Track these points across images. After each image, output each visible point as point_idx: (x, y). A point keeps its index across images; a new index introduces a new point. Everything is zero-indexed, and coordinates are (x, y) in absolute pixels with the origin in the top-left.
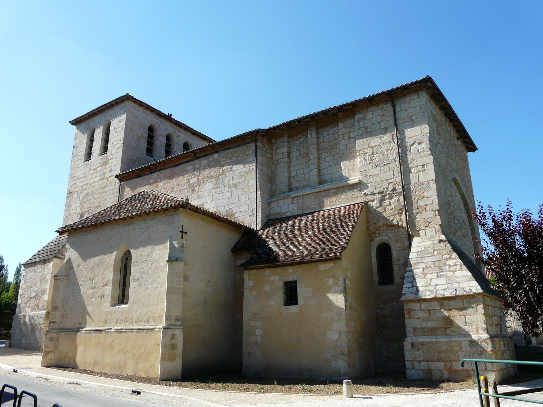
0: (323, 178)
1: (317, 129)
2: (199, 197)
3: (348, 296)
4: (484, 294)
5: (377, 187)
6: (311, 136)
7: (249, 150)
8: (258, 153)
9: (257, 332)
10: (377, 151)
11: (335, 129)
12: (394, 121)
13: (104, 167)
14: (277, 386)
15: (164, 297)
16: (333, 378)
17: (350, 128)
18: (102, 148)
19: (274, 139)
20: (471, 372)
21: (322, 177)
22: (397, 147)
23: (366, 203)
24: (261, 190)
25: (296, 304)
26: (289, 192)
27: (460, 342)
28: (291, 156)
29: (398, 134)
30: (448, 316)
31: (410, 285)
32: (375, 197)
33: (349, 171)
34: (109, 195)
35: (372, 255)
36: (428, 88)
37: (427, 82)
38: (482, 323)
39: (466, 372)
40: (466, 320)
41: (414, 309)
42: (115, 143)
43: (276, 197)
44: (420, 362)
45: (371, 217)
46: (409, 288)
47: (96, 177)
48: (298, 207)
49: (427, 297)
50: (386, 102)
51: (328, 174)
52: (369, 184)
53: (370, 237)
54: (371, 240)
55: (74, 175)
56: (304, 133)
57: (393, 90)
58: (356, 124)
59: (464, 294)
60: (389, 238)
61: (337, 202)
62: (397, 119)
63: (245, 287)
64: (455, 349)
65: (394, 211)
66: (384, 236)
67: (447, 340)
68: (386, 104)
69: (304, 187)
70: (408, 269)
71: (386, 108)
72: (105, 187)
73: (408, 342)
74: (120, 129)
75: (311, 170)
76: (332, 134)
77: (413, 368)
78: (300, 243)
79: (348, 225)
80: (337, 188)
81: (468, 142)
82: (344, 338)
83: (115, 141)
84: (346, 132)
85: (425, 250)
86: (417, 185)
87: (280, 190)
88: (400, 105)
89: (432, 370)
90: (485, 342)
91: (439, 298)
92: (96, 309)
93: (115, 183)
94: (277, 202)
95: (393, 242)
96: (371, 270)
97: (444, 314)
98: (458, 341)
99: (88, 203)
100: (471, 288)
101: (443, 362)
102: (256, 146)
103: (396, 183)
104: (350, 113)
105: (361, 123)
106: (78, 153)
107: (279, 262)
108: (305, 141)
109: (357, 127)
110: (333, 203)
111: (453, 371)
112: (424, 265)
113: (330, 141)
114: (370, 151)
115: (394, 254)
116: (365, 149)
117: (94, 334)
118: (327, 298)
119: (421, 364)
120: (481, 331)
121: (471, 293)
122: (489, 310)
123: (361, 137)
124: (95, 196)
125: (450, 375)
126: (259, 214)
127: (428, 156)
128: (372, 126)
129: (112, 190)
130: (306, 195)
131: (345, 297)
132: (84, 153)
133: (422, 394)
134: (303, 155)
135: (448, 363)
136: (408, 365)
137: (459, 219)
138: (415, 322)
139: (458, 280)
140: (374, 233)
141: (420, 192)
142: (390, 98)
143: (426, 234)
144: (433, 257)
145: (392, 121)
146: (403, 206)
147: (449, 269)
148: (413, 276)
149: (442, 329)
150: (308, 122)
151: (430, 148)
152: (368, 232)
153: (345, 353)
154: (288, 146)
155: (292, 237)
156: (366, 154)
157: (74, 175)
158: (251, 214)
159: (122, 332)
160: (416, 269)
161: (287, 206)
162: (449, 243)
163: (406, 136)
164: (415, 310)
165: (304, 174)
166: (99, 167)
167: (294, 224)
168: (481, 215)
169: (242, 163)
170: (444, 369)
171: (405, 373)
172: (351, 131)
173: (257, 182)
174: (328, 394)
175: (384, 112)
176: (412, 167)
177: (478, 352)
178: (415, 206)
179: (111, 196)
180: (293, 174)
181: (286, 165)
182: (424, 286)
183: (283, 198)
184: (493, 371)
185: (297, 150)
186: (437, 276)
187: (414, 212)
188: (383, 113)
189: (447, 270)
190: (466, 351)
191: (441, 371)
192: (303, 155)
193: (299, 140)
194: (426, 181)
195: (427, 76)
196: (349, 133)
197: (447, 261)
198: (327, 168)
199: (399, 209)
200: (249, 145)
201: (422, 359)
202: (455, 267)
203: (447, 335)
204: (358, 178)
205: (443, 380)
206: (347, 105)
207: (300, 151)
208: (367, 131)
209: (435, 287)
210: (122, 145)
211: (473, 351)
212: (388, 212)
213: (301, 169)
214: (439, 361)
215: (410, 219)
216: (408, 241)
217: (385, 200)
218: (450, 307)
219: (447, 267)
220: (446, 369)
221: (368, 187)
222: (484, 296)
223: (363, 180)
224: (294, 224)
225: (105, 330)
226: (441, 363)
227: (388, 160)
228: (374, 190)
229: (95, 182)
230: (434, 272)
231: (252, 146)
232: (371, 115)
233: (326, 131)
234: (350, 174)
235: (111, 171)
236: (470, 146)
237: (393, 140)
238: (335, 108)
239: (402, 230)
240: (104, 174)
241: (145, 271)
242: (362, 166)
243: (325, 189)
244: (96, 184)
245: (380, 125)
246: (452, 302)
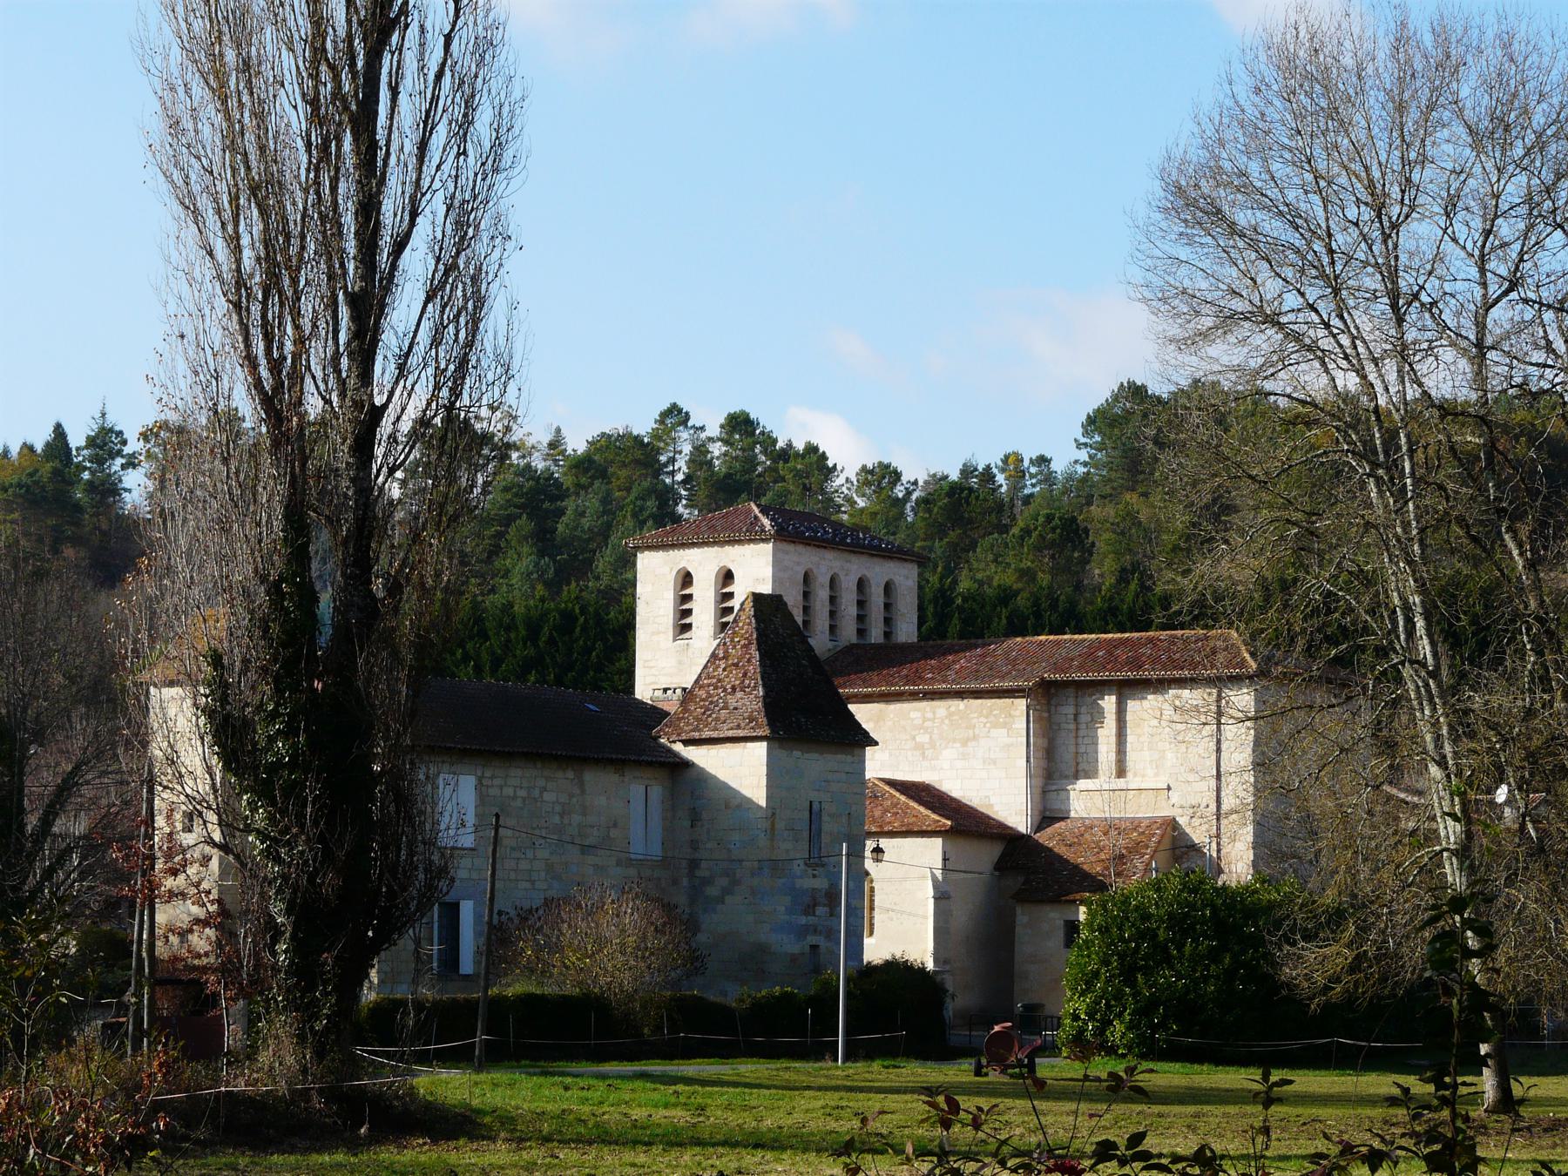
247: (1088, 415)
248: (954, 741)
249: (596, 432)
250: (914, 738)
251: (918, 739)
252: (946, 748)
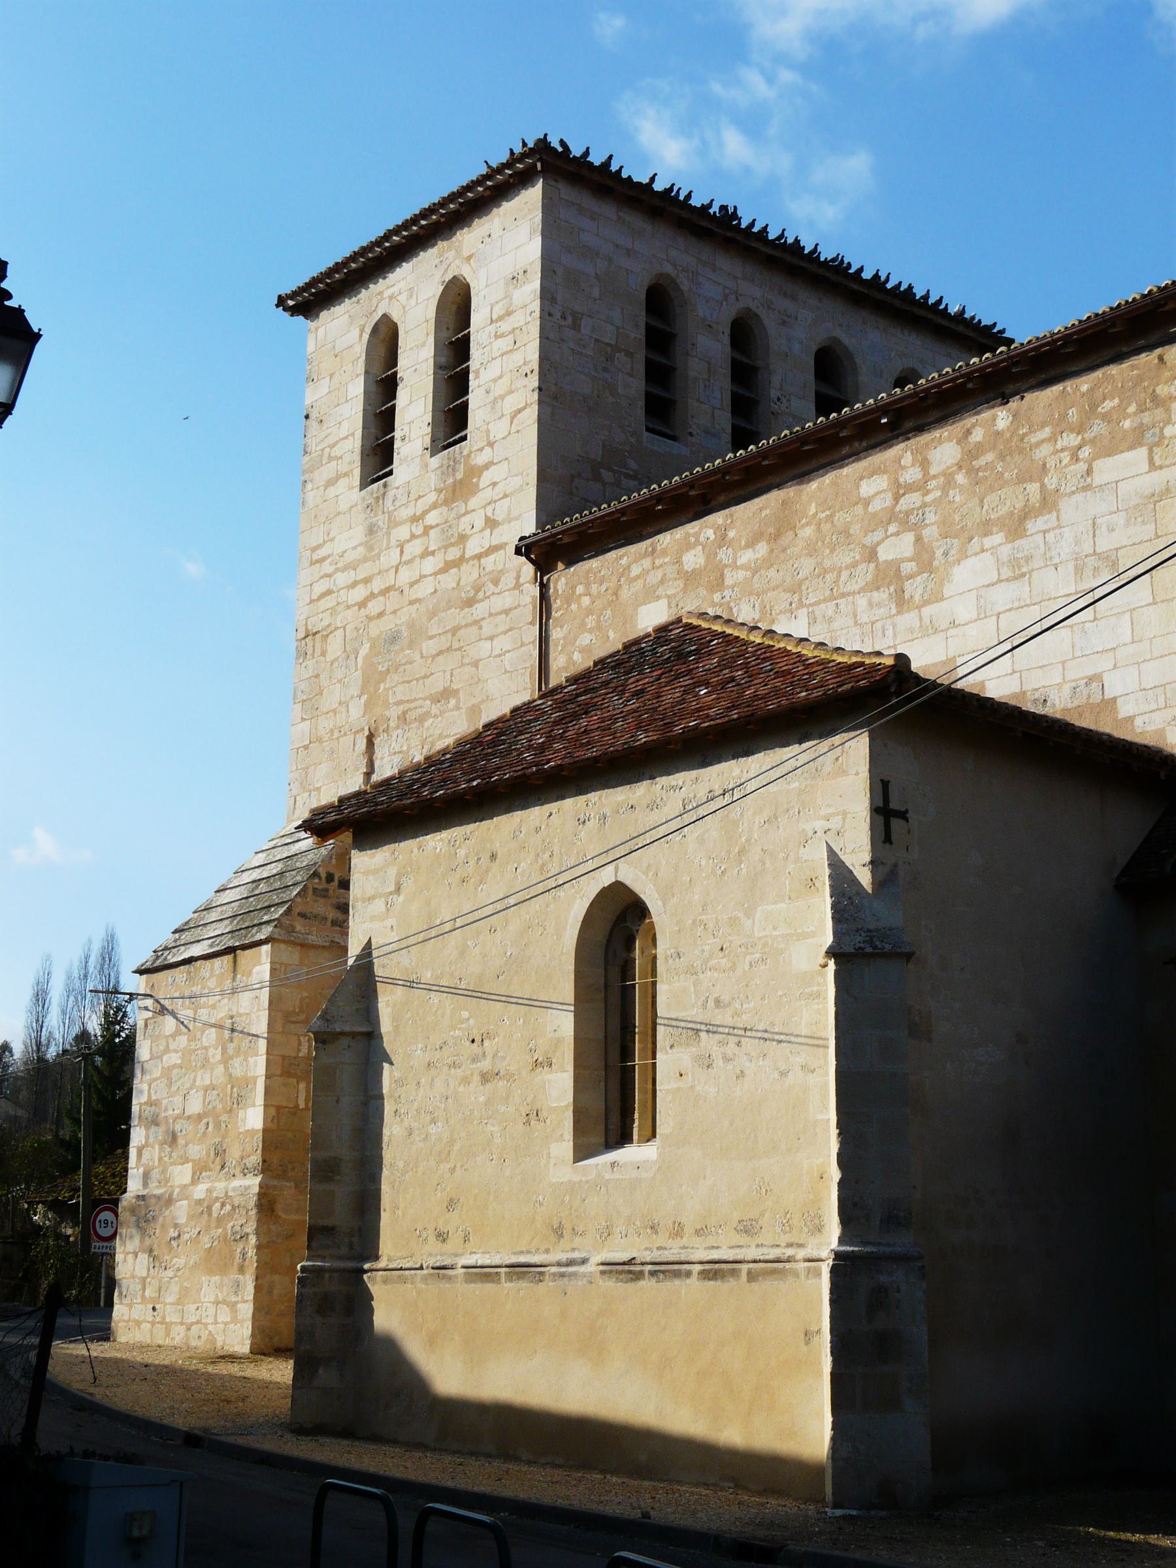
2: (930, 629)
13: (460, 506)
15: (819, 1117)
18: (442, 417)
34: (491, 638)
42: (499, 389)
47: (426, 553)
55: (321, 553)
72: (470, 602)
74: (518, 319)
83: (501, 377)
92: (508, 1173)
93: (518, 577)
99: (395, 677)
106: (332, 446)
117: (509, 1285)
124: (429, 647)
129: (506, 612)
132: (358, 443)
157: (321, 553)
159: (638, 1276)
166: (434, 506)
179: (503, 643)
210: (536, 396)
225: (559, 1264)
229: (422, 577)
235: (491, 523)
240: (463, 538)
241: (725, 998)
244: (425, 589)
247: (292, 315)
248: (986, 528)
249: (451, 191)
250: (871, 554)
251: (884, 554)
252: (964, 555)
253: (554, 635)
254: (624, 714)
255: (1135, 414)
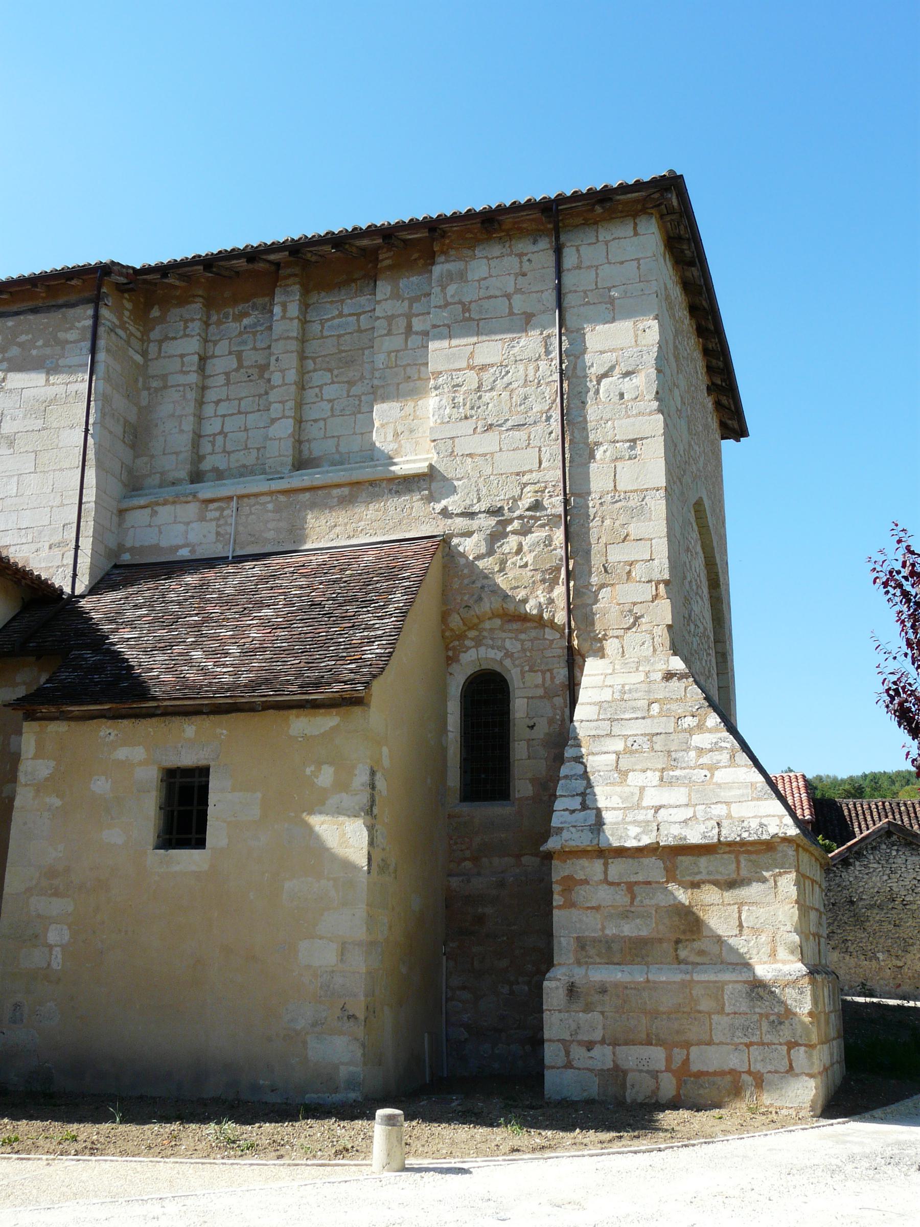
0: (311, 453)
1: (306, 291)
3: (377, 827)
4: (805, 842)
5: (484, 491)
6: (285, 310)
7: (71, 329)
8: (101, 343)
9: (53, 936)
10: (494, 381)
11: (362, 300)
12: (554, 294)
14: (122, 1128)
16: (311, 1097)
17: (413, 300)
19: (156, 307)
20: (745, 1077)
21: (307, 444)
22: (556, 376)
23: (445, 540)
24: (100, 466)
25: (200, 843)
26: (192, 482)
27: (720, 987)
28: (209, 370)
29: (564, 338)
30: (687, 903)
31: (576, 803)
32: (475, 524)
33: (396, 435)
35: (449, 703)
36: (665, 211)
37: (668, 190)
38: (789, 928)
39: (728, 1078)
40: (743, 918)
41: (584, 877)
43: (146, 495)
44: (590, 1046)
45: (456, 586)
46: (573, 811)
48: (218, 534)
49: (631, 843)
50: (535, 235)
51: (325, 437)
52: (460, 483)
53: (447, 648)
54: (448, 658)
56: (260, 301)
57: (561, 199)
58: (436, 290)
59: (742, 839)
60: (508, 655)
61: (350, 528)
62: (563, 292)
63: (22, 778)
64: (701, 1008)
65: (532, 573)
66: (493, 648)
67: (678, 977)
68: (535, 242)
69: (245, 471)
70: (569, 753)
71: (533, 253)
73: (558, 983)
75: (273, 421)
76: (350, 315)
77: (569, 1065)
78: (225, 644)
79: (388, 602)
80: (356, 484)
81: (729, 409)
82: (359, 964)
84: (399, 313)
85: (622, 700)
86: (608, 498)
87: (162, 474)
88: (578, 250)
89: (625, 1073)
90: (793, 988)
91: (664, 847)
94: (148, 510)
95: (519, 669)
96: (444, 750)
97: (675, 898)
98: (716, 982)
100: (764, 821)
101: (661, 1046)
102: (96, 317)
103: (546, 487)
104: (416, 255)
105: (451, 289)
107: (154, 699)
108: (261, 325)
109: (436, 299)
110: (337, 530)
111: (690, 1076)
112: (619, 745)
113: (343, 335)
114: (471, 379)
115: (519, 707)
116: (455, 370)
118: (309, 829)
119: (593, 1053)
120: (782, 953)
121: (765, 837)
122: (805, 890)
123: (448, 331)
125: (679, 1087)
126: (86, 544)
127: (650, 414)
128: (486, 304)
130: (248, 496)
131: (371, 829)
133: (622, 1153)
134: (250, 371)
135: (676, 1050)
136: (551, 1053)
137: (700, 625)
138: (584, 918)
139: (725, 795)
140: (461, 637)
141: (618, 523)
142: (550, 226)
143: (623, 652)
144: (648, 721)
145: (550, 297)
146: (561, 560)
147: (697, 761)
148: (585, 775)
149: (665, 945)
150: (277, 265)
151: (657, 393)
152: (443, 631)
153: (358, 1015)
154: (203, 335)
155: (197, 625)
156: (458, 385)
158: (56, 539)
160: (593, 754)
161: (181, 528)
162: (696, 682)
163: (587, 345)
164: (586, 882)
165: (246, 430)
167: (203, 586)
168: (905, 572)
169: (44, 368)
170: (663, 1068)
171: (540, 1078)
172: (414, 311)
173: (89, 437)
174: (314, 1156)
175: (526, 265)
176: (598, 444)
177: (772, 1018)
178: (596, 561)
180: (211, 427)
181: (191, 395)
182: (620, 809)
183: (171, 499)
184: (811, 1076)
185: (230, 353)
186: (661, 779)
187: (594, 580)
188: (521, 267)
189: (692, 764)
190: (735, 1013)
191: (655, 1074)
192: (250, 371)
193: (241, 321)
194: (636, 491)
195: (671, 171)
196: (409, 317)
197: (691, 735)
198: (324, 420)
199: (547, 567)
200: (71, 312)
201: (599, 1038)
202: (716, 756)
203: (679, 961)
204: (426, 460)
205: (657, 1101)
206: (413, 225)
207: (239, 356)
208: (467, 315)
209: (656, 812)
211: (755, 1013)
212: (511, 575)
213: (240, 413)
214: (651, 1044)
215: (578, 602)
216: (566, 669)
217: (505, 535)
218: (697, 878)
219: (693, 754)
220: (668, 1069)
221: (454, 490)
222: (798, 846)
223: (441, 467)
224: (203, 586)
226: (655, 1048)
227: (526, 413)
228: (475, 501)
230: (650, 765)
231: (83, 317)
232: (486, 268)
233: (332, 302)
234: (400, 446)
236: (730, 422)
237: (548, 352)
238: (372, 231)
239: (549, 634)
242: (442, 423)
243: (316, 483)
245: (510, 304)
246: (703, 861)
253: (727, 894)
254: (190, 665)
255: (42, 347)
